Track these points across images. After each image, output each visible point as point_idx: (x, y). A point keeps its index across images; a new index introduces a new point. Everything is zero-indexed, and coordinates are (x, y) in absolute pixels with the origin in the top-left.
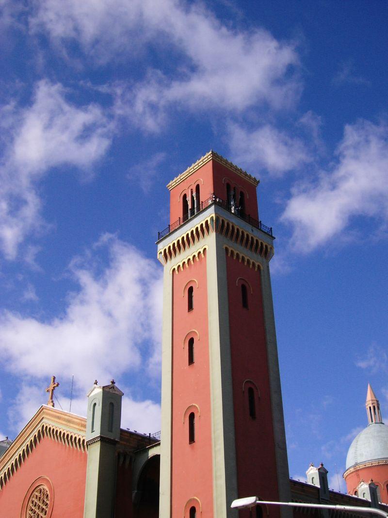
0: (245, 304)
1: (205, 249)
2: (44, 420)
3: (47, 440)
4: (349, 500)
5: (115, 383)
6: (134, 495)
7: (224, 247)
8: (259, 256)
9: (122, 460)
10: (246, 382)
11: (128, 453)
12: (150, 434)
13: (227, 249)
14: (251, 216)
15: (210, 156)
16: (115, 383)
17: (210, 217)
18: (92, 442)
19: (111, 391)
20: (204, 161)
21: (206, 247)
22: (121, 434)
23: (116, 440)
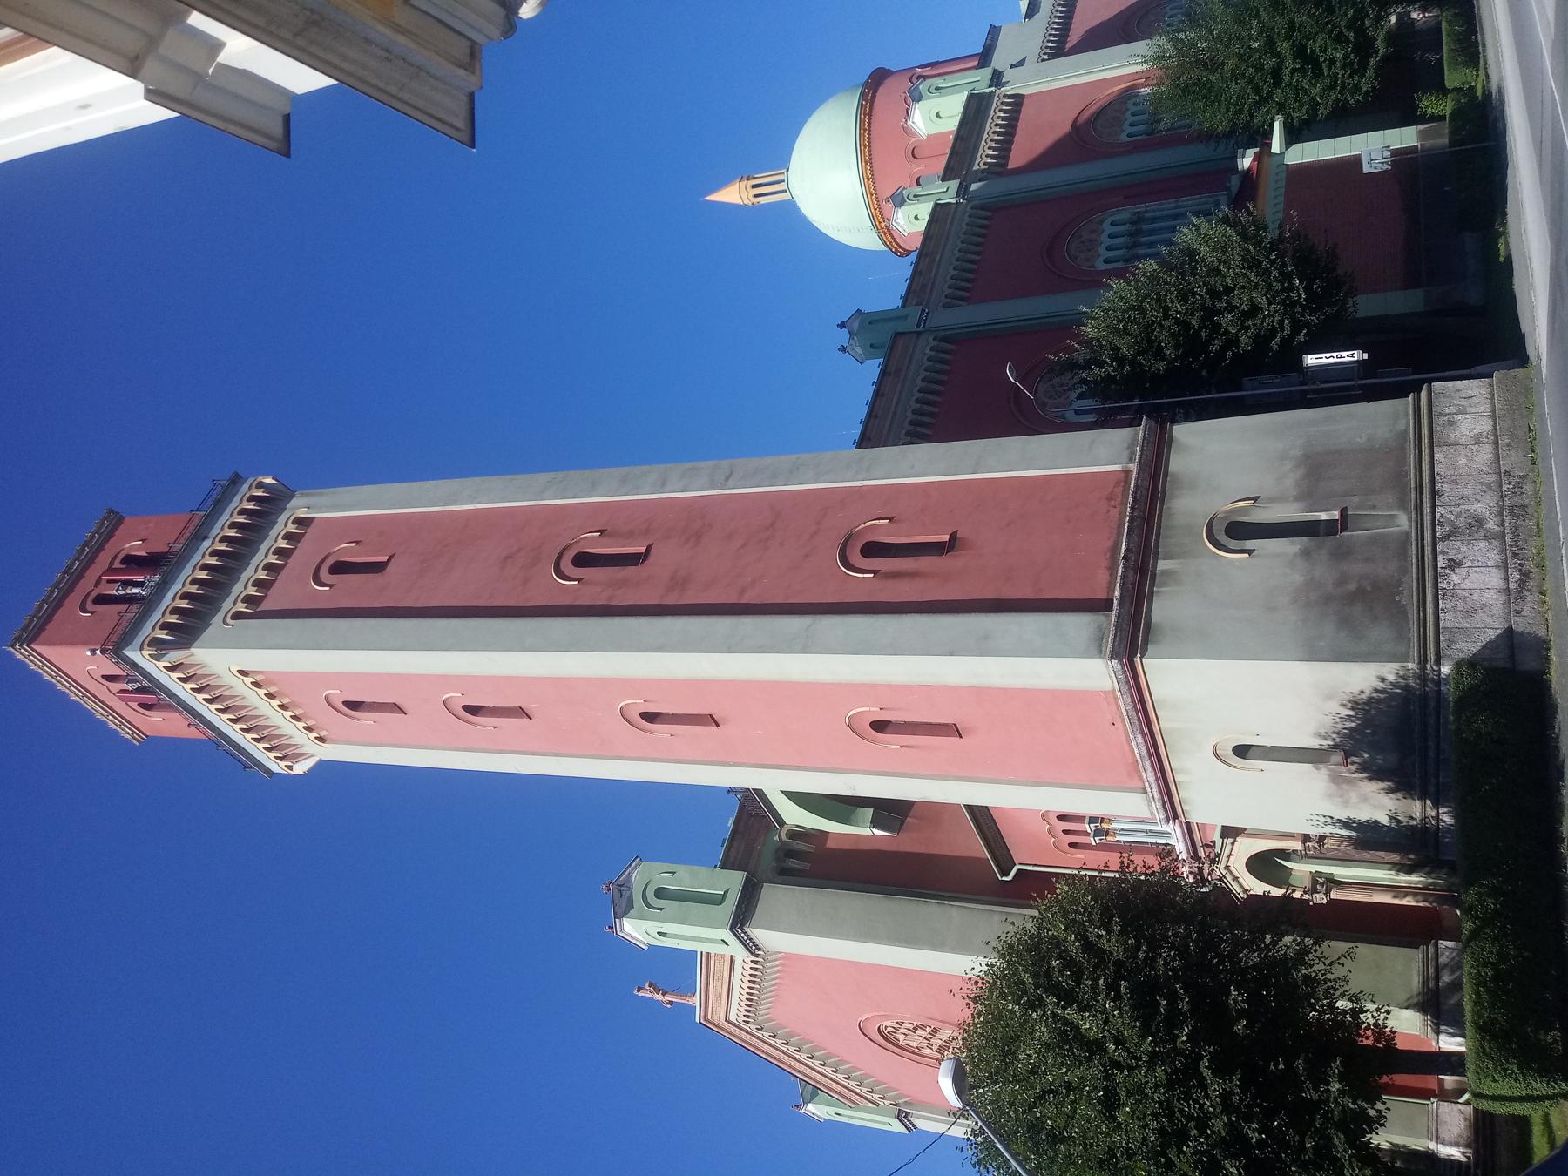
2: (732, 1018)
4: (926, 255)
9: (792, 863)
13: (238, 616)
18: (751, 946)
21: (234, 670)
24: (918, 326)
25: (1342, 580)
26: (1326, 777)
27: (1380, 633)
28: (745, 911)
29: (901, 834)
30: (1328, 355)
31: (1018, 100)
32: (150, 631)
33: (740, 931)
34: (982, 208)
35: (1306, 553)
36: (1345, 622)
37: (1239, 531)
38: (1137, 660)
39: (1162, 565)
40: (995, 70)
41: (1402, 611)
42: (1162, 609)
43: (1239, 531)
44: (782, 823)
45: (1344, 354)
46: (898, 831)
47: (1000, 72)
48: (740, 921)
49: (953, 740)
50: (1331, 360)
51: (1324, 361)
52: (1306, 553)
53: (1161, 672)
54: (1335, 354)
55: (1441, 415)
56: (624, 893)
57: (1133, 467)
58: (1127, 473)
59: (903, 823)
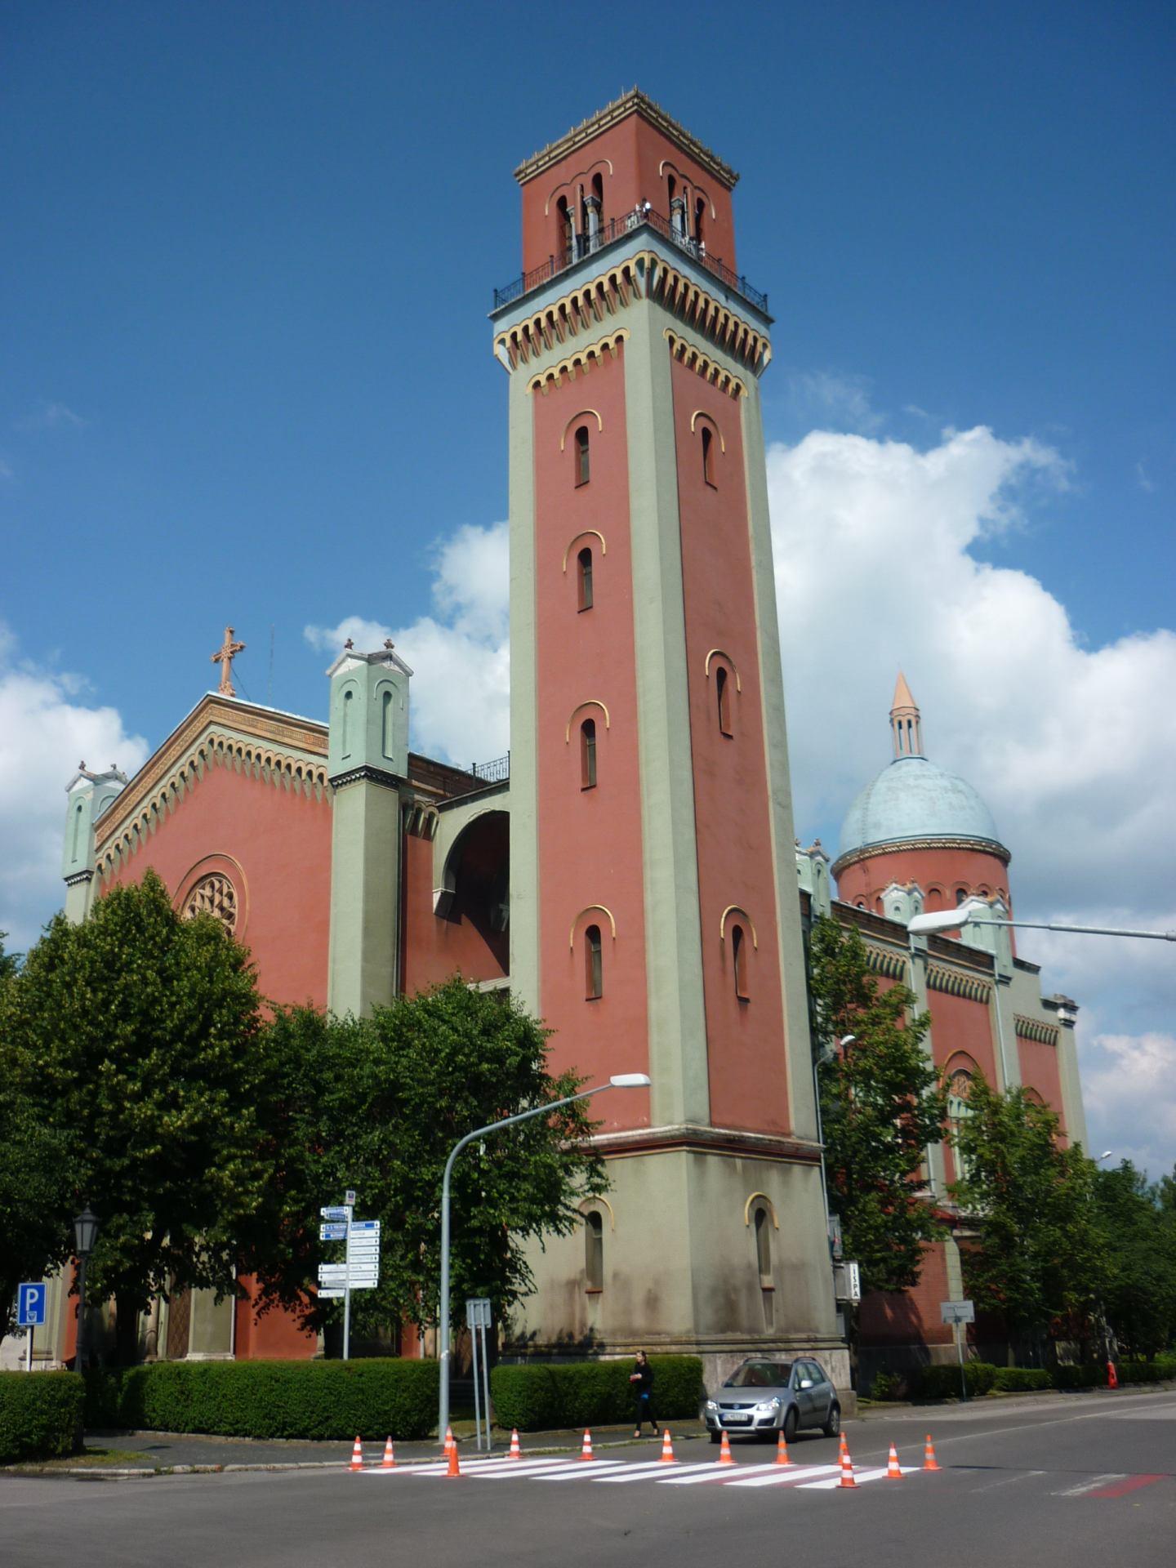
1: (620, 339)
2: (212, 728)
3: (717, 1119)
4: (869, 921)
5: (392, 647)
6: (436, 897)
12: (474, 764)
14: (723, 262)
15: (631, 104)
16: (392, 647)
17: (635, 260)
18: (340, 781)
20: (602, 123)
22: (410, 764)
25: (736, 1290)
26: (572, 1277)
27: (708, 1316)
29: (434, 916)
30: (857, 1278)
31: (986, 1002)
32: (681, 172)
33: (363, 774)
34: (902, 968)
35: (749, 1266)
36: (714, 1291)
37: (761, 1215)
38: (685, 1148)
39: (739, 1162)
40: (1010, 979)
41: (723, 1331)
42: (713, 1162)
43: (761, 1215)
44: (442, 809)
45: (858, 1290)
46: (437, 913)
47: (1008, 983)
48: (373, 775)
49: (582, 991)
50: (853, 1280)
51: (852, 1275)
52: (749, 1266)
53: (680, 1161)
54: (858, 1283)
55: (831, 1355)
57: (793, 1140)
58: (789, 1135)
59: (444, 918)
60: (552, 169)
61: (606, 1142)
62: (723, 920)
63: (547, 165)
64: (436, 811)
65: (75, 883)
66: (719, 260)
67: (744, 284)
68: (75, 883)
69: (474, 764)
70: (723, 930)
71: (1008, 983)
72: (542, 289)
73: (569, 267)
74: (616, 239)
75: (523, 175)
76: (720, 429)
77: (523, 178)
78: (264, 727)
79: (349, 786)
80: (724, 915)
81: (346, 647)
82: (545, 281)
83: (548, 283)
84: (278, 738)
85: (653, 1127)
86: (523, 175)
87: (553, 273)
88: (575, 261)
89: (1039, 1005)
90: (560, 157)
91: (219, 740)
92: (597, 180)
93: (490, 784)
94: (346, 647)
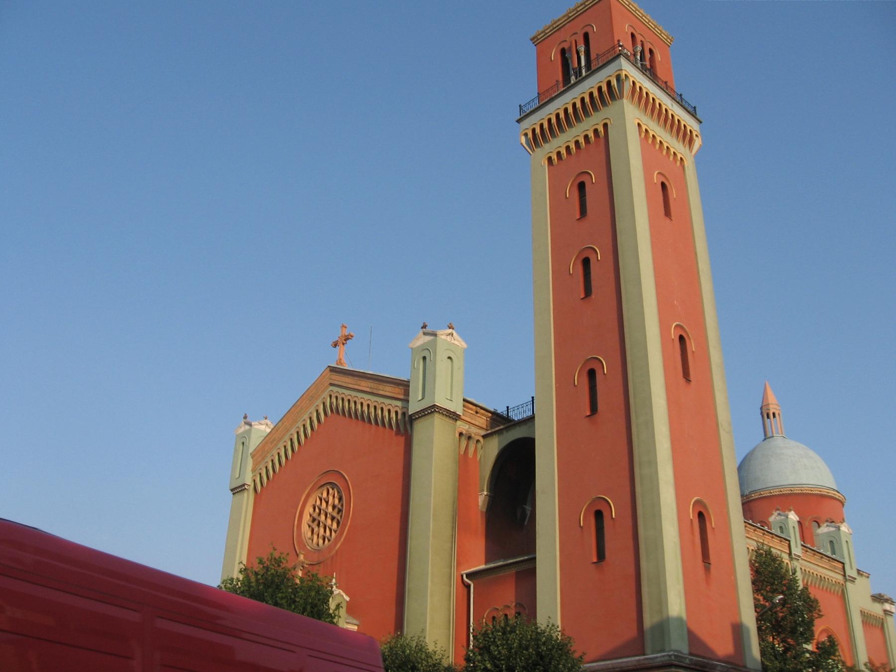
0: (668, 213)
7: (637, 121)
8: (681, 144)
10: (674, 328)
11: (473, 435)
12: (508, 407)
19: (449, 340)
23: (458, 413)
24: (849, 576)
28: (443, 414)
40: (855, 579)
56: (448, 337)
60: (555, 34)
61: (611, 666)
62: (691, 506)
63: (552, 32)
64: (481, 440)
65: (238, 492)
66: (666, 83)
67: (681, 98)
68: (238, 492)
69: (508, 407)
70: (692, 515)
71: (854, 582)
72: (552, 100)
73: (569, 85)
74: (599, 66)
75: (535, 40)
76: (671, 181)
77: (536, 41)
78: (365, 385)
79: (423, 419)
80: (692, 504)
81: (422, 328)
82: (553, 96)
83: (555, 96)
84: (375, 391)
85: (646, 655)
86: (535, 40)
87: (558, 91)
88: (584, 74)
89: (870, 599)
90: (560, 26)
91: (335, 395)
92: (586, 36)
93: (513, 420)
94: (422, 328)
